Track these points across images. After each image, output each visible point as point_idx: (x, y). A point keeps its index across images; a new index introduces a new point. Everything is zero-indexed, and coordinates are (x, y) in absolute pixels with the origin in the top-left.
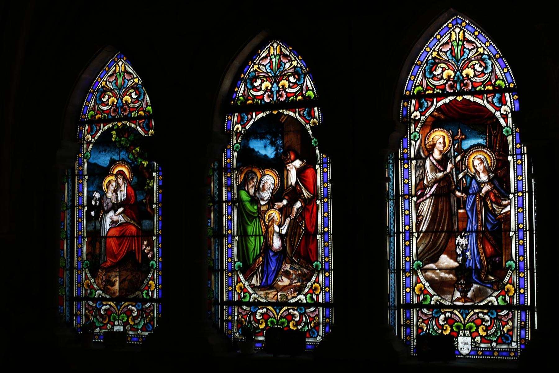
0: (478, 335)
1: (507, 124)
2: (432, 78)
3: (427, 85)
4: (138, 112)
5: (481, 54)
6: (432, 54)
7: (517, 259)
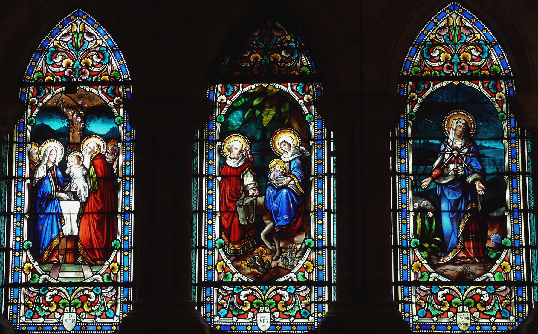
0: (476, 310)
1: (119, 113)
2: (52, 65)
3: (47, 72)
4: (101, 77)
5: (477, 39)
6: (54, 43)
7: (316, 238)
